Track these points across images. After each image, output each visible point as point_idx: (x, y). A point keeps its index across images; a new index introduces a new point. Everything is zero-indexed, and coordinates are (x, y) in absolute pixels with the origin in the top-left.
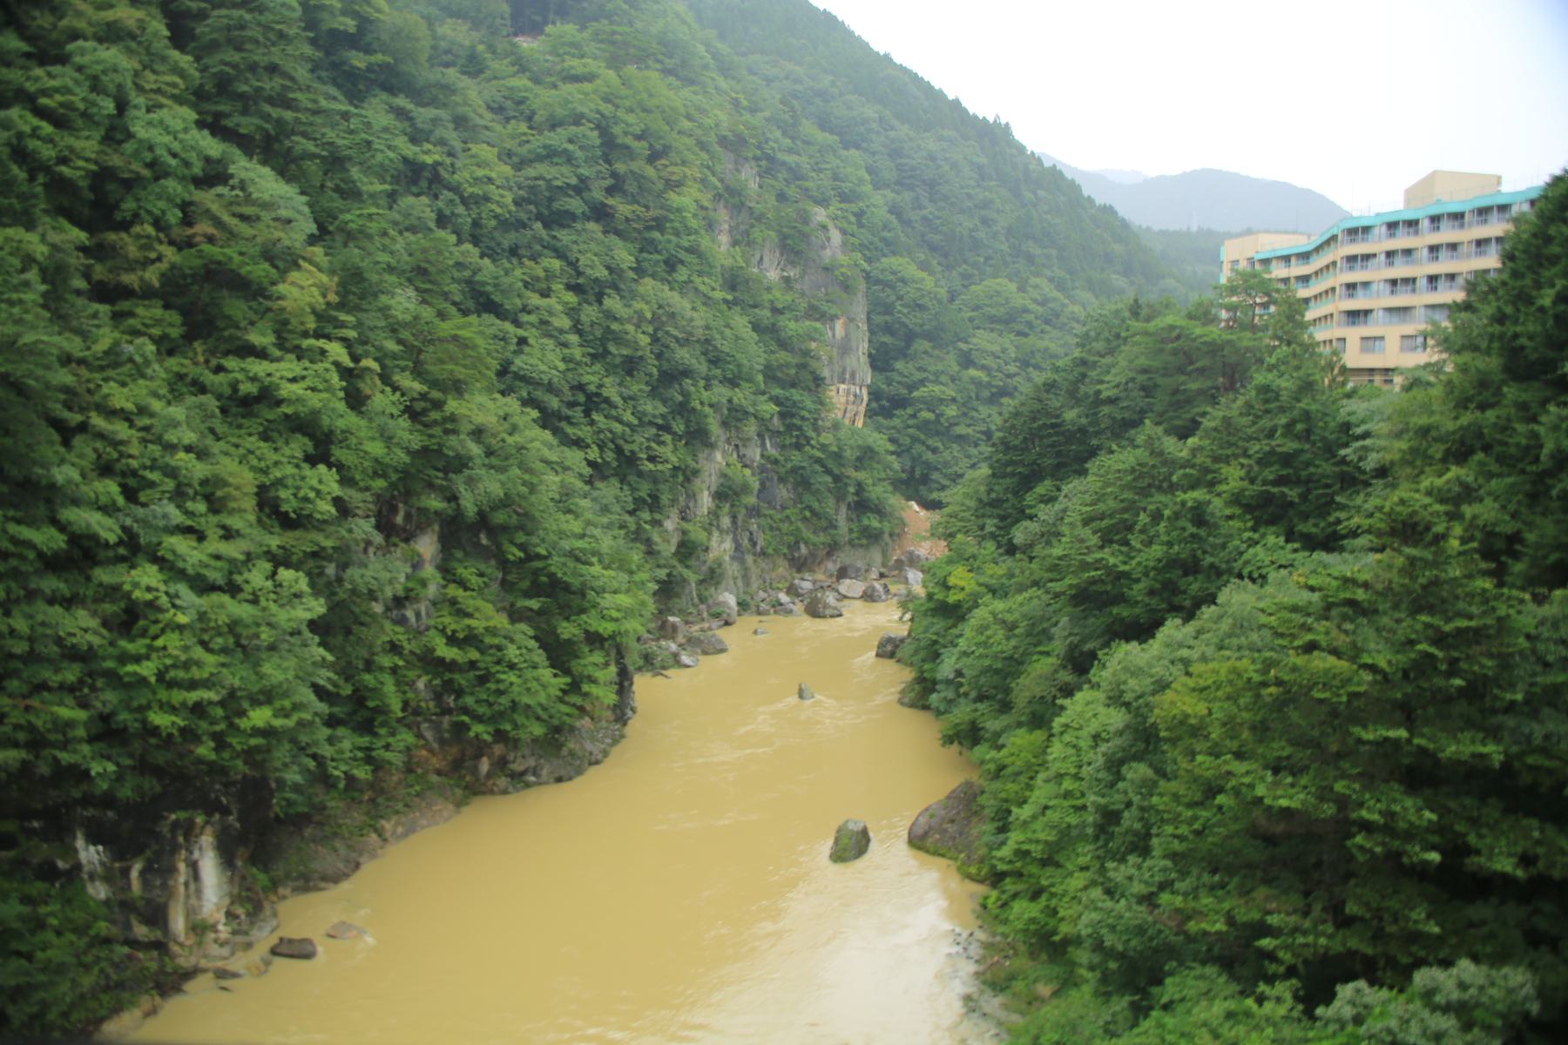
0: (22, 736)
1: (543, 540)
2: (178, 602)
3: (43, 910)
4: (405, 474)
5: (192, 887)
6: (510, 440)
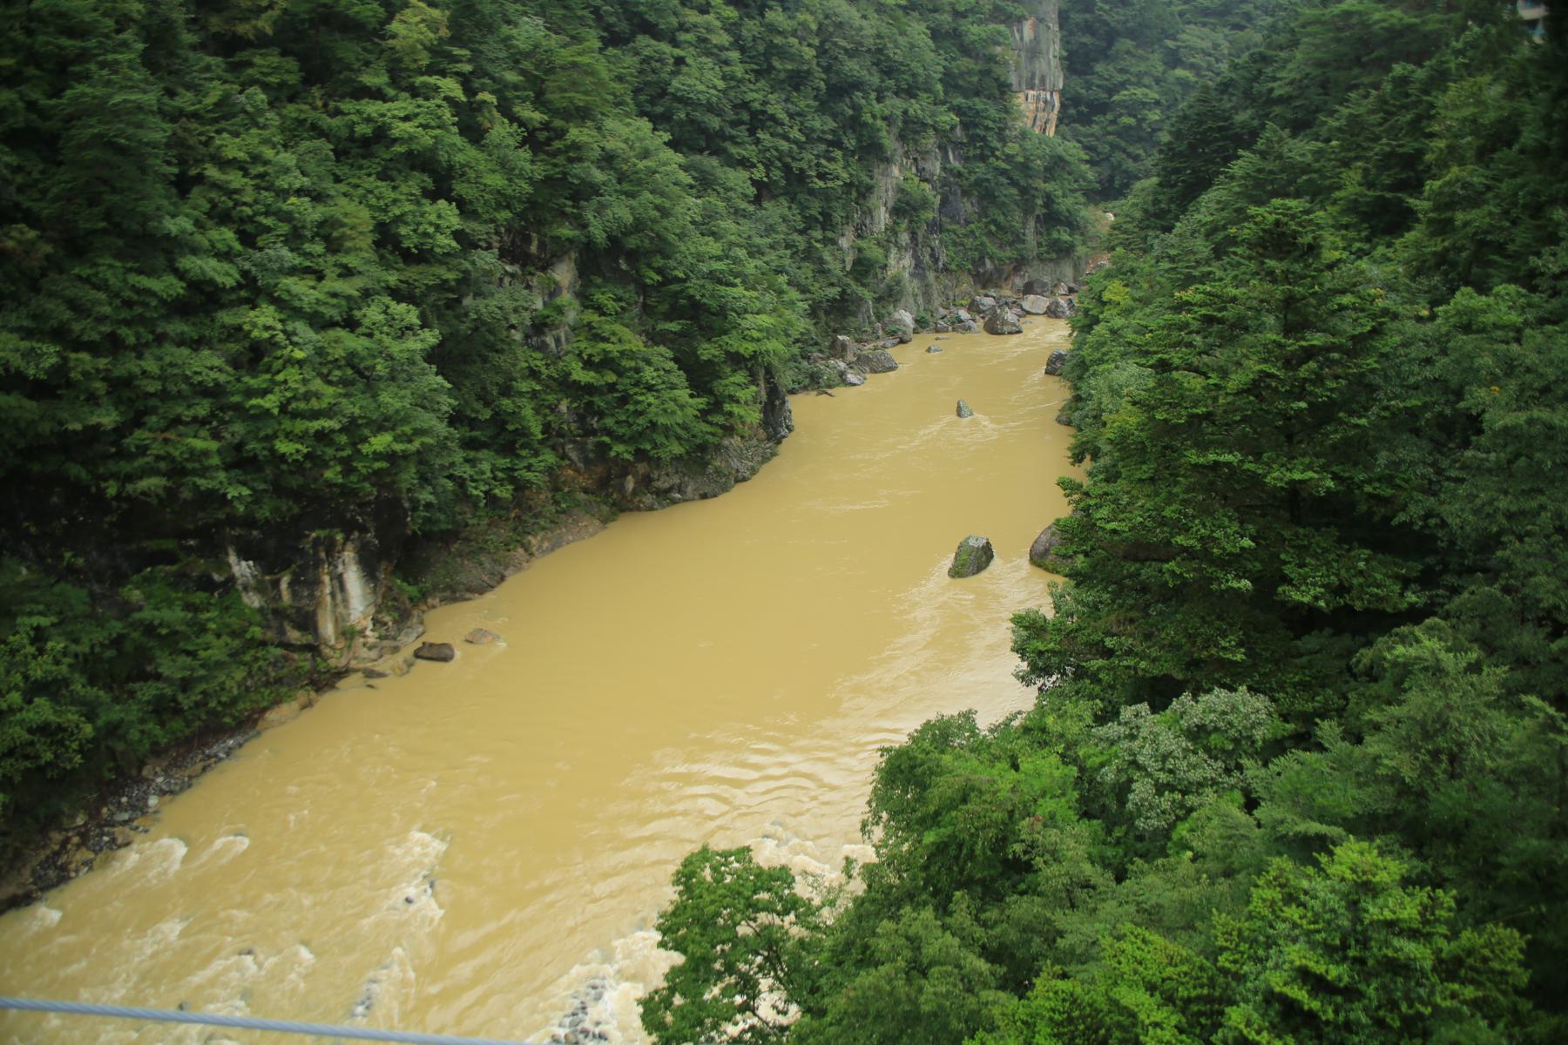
0: (163, 465)
1: (681, 263)
2: (295, 339)
3: (204, 616)
4: (532, 204)
5: (339, 597)
6: (641, 165)
